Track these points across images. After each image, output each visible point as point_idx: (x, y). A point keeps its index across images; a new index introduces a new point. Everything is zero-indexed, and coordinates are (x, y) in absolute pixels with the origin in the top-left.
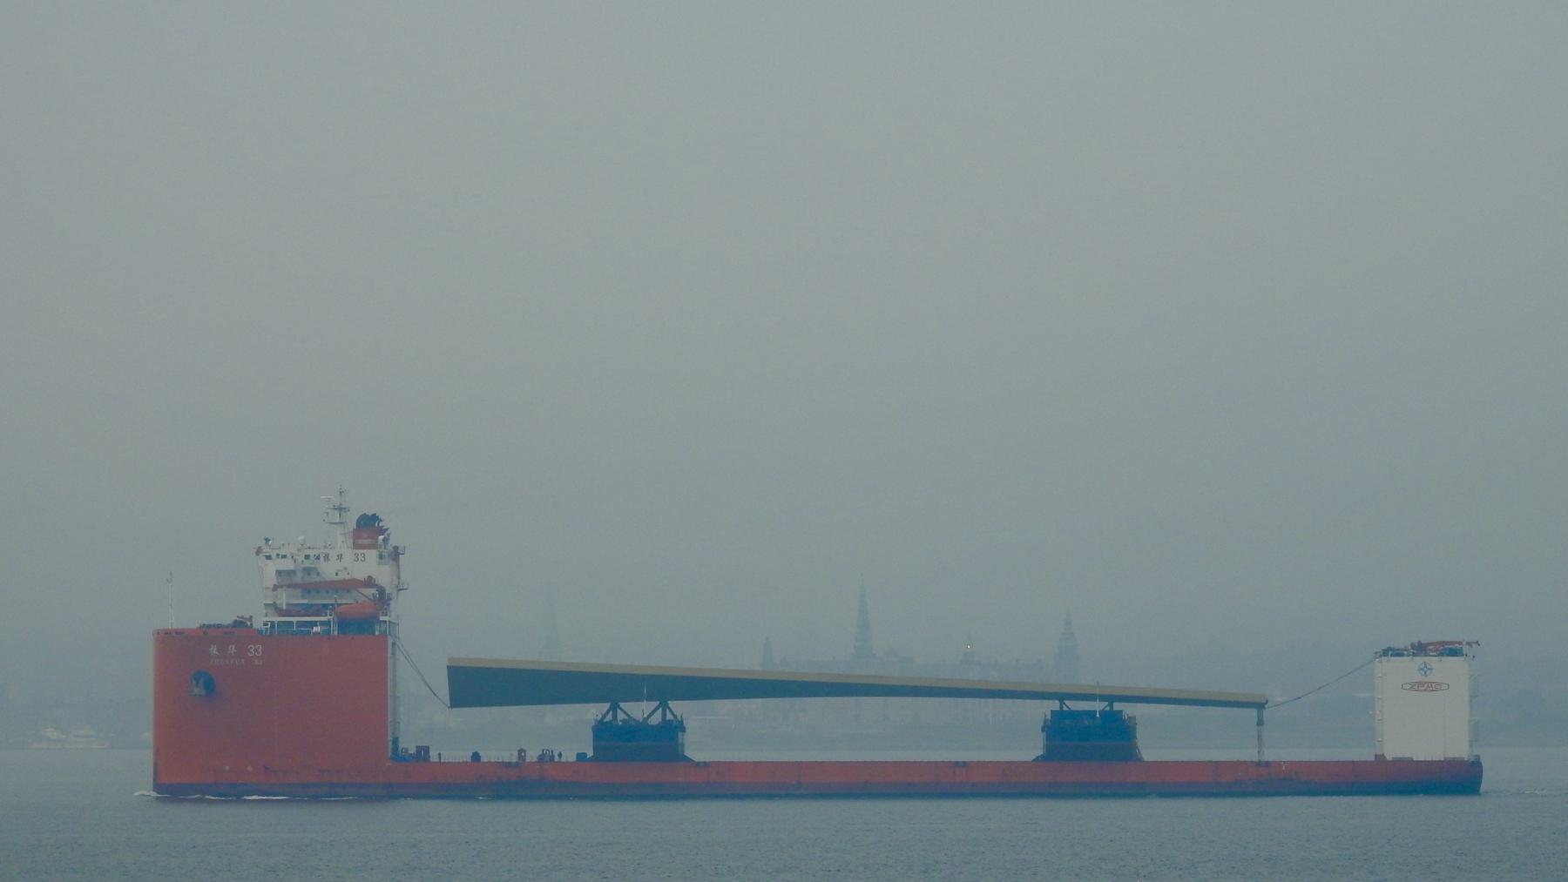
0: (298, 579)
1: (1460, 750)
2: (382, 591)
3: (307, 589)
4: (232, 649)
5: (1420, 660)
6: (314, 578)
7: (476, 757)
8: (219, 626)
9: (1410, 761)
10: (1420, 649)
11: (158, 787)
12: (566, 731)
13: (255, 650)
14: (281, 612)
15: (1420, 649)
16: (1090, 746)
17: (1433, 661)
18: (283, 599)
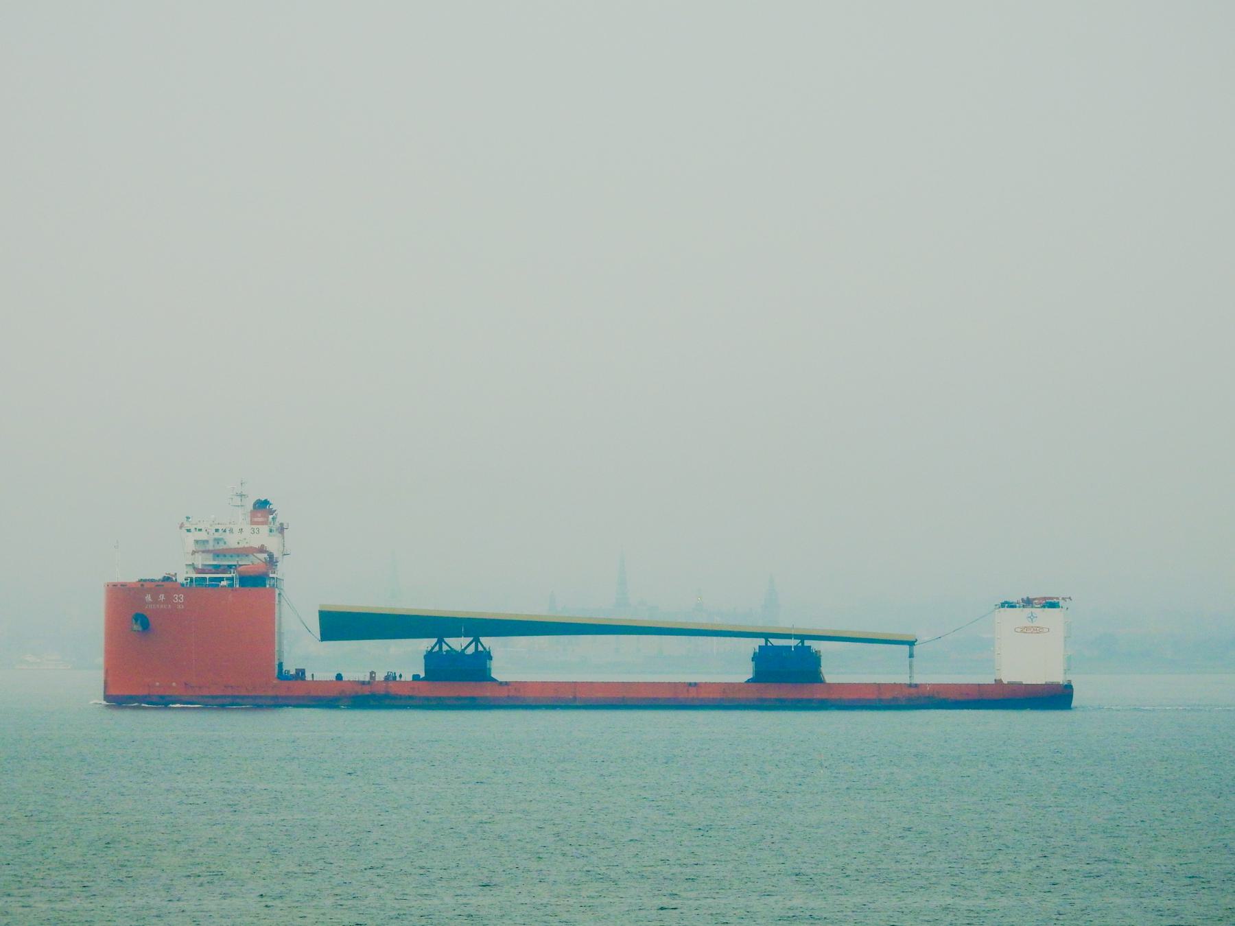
0: (210, 546)
1: (1059, 678)
2: (271, 556)
3: (217, 554)
5: (1028, 610)
6: (221, 546)
7: (339, 677)
8: (152, 581)
9: (1020, 684)
10: (1028, 602)
11: (107, 697)
12: (404, 659)
13: (179, 598)
15: (1028, 602)
16: (787, 674)
17: (1038, 611)
18: (200, 561)
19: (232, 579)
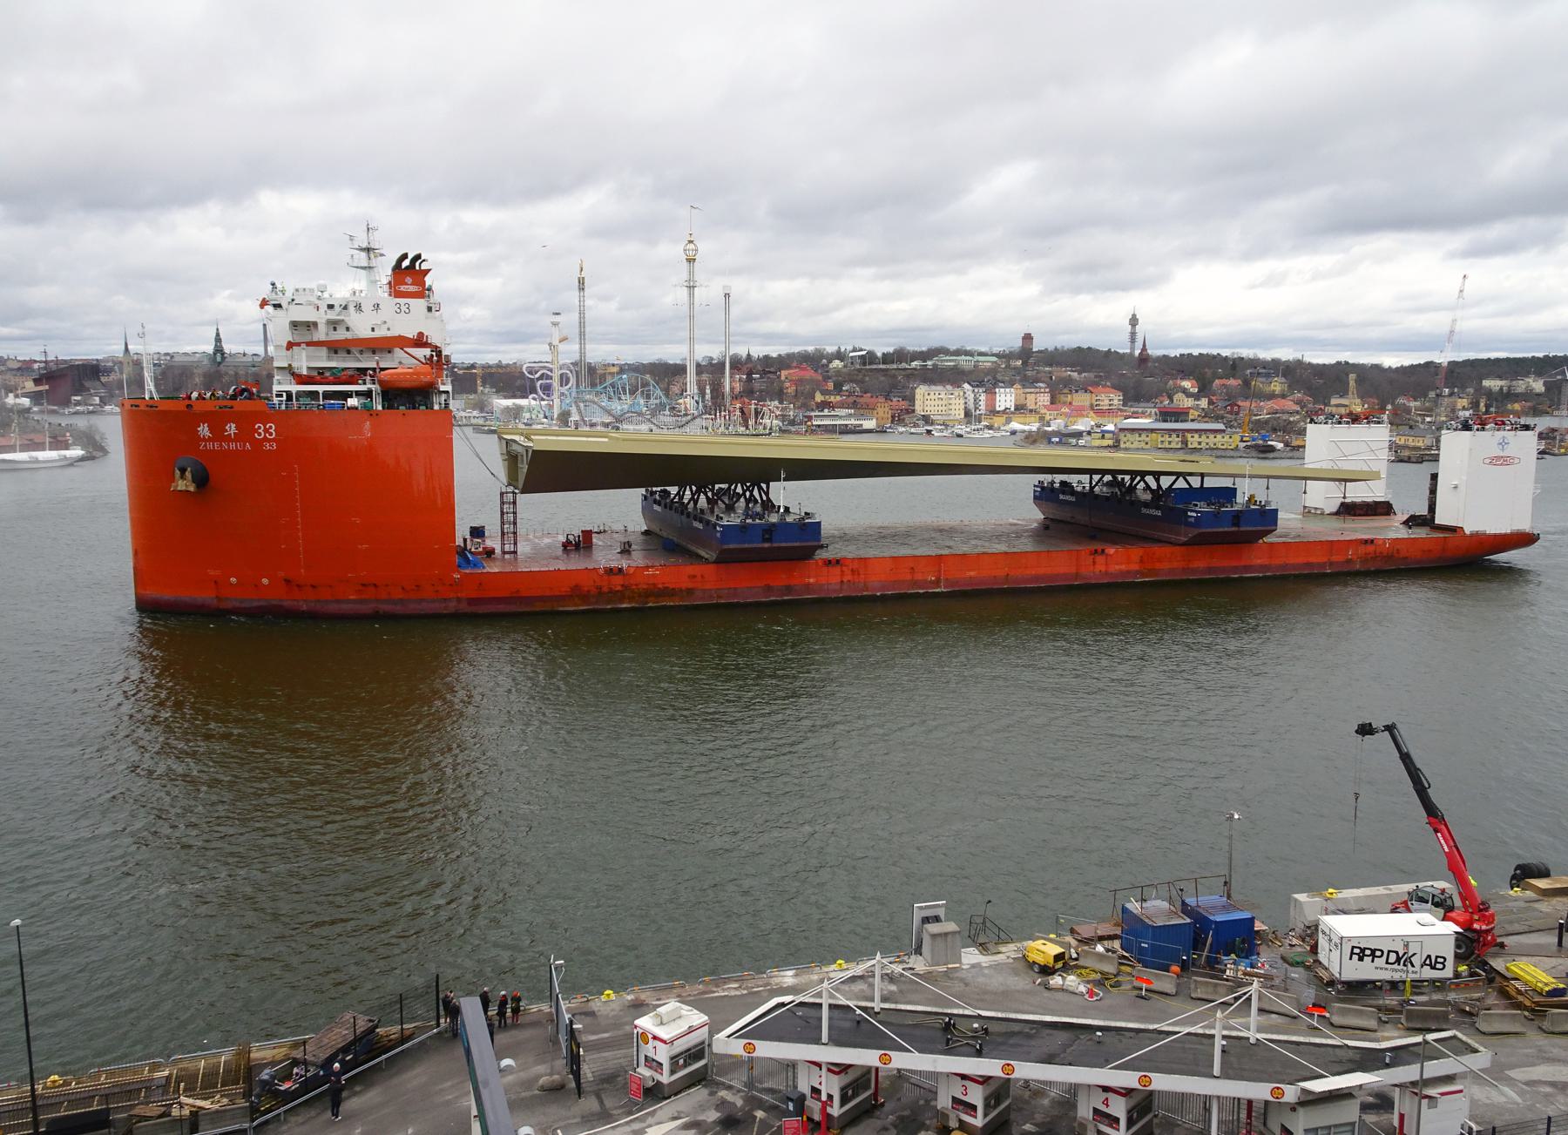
0: (321, 334)
3: (334, 348)
6: (341, 335)
14: (301, 380)
19: (368, 394)
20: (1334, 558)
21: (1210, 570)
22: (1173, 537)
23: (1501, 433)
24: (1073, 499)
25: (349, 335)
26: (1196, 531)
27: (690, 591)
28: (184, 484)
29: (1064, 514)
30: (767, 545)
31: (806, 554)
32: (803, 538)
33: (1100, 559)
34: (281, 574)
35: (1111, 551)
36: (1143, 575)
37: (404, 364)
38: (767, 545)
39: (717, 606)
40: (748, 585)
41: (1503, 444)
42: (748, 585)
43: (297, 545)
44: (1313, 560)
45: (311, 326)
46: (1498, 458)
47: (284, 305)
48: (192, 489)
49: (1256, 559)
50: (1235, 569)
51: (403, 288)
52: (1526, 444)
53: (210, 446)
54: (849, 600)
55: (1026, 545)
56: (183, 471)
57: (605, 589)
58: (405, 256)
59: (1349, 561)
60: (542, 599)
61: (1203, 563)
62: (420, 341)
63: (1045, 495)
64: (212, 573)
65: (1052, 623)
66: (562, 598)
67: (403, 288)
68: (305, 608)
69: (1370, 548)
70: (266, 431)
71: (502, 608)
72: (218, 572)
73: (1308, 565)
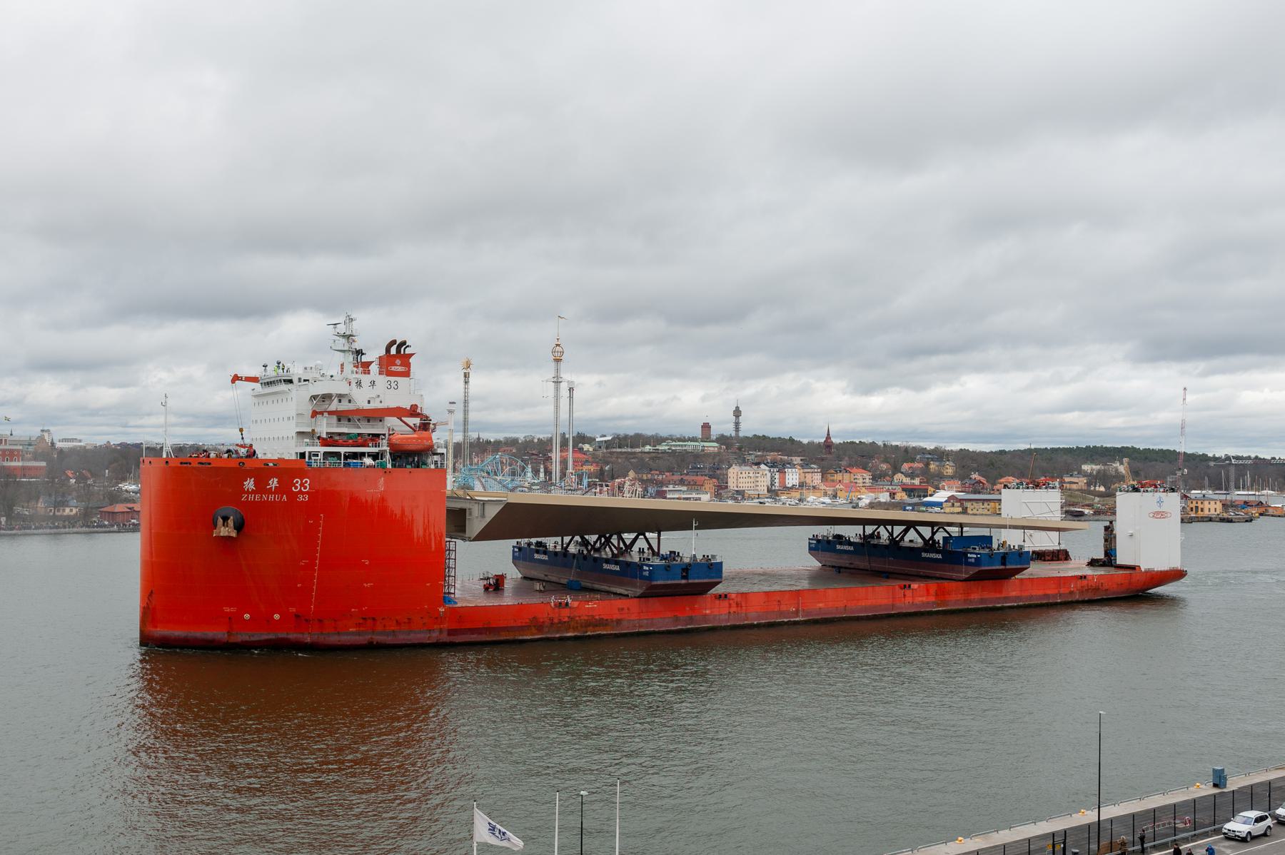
0: (334, 406)
3: (341, 416)
4: (274, 483)
6: (344, 406)
13: (302, 486)
14: (325, 442)
18: (325, 426)
19: (375, 456)
20: (1062, 591)
21: (982, 601)
22: (955, 575)
23: (1157, 495)
24: (545, 558)
25: (351, 407)
26: (977, 569)
27: (619, 621)
28: (225, 531)
29: (844, 561)
30: (684, 581)
31: (704, 589)
32: (699, 579)
33: (908, 593)
34: (293, 610)
35: (915, 586)
36: (938, 605)
37: (399, 429)
38: (684, 581)
39: (639, 634)
40: (662, 618)
41: (1160, 502)
42: (662, 618)
43: (289, 591)
44: (1049, 592)
45: (326, 397)
46: (1158, 513)
47: (295, 380)
48: (234, 534)
49: (1012, 592)
50: (998, 600)
51: (393, 368)
52: (1173, 502)
53: (251, 498)
54: (734, 627)
55: (804, 585)
56: (225, 519)
57: (556, 621)
58: (393, 342)
59: (1071, 593)
60: (507, 629)
61: (980, 596)
62: (413, 412)
63: (818, 546)
64: (227, 610)
65: (941, 633)
66: (522, 629)
67: (393, 368)
68: (309, 640)
69: (1085, 582)
70: (302, 485)
71: (474, 637)
72: (233, 610)
73: (1046, 596)
